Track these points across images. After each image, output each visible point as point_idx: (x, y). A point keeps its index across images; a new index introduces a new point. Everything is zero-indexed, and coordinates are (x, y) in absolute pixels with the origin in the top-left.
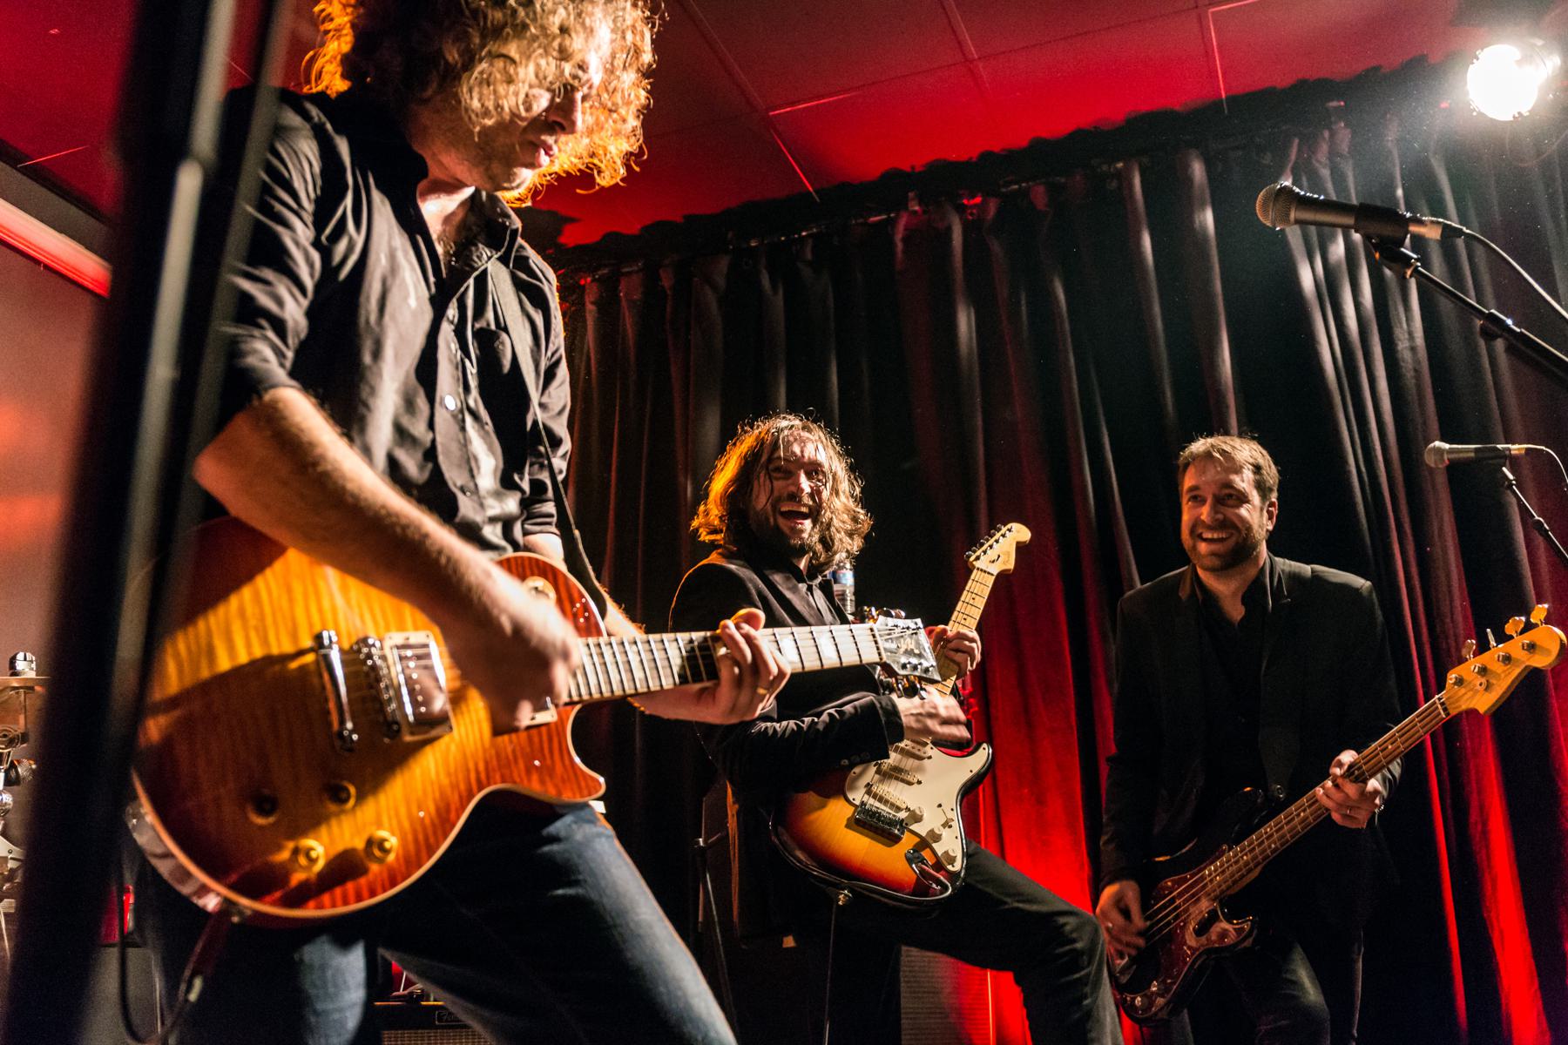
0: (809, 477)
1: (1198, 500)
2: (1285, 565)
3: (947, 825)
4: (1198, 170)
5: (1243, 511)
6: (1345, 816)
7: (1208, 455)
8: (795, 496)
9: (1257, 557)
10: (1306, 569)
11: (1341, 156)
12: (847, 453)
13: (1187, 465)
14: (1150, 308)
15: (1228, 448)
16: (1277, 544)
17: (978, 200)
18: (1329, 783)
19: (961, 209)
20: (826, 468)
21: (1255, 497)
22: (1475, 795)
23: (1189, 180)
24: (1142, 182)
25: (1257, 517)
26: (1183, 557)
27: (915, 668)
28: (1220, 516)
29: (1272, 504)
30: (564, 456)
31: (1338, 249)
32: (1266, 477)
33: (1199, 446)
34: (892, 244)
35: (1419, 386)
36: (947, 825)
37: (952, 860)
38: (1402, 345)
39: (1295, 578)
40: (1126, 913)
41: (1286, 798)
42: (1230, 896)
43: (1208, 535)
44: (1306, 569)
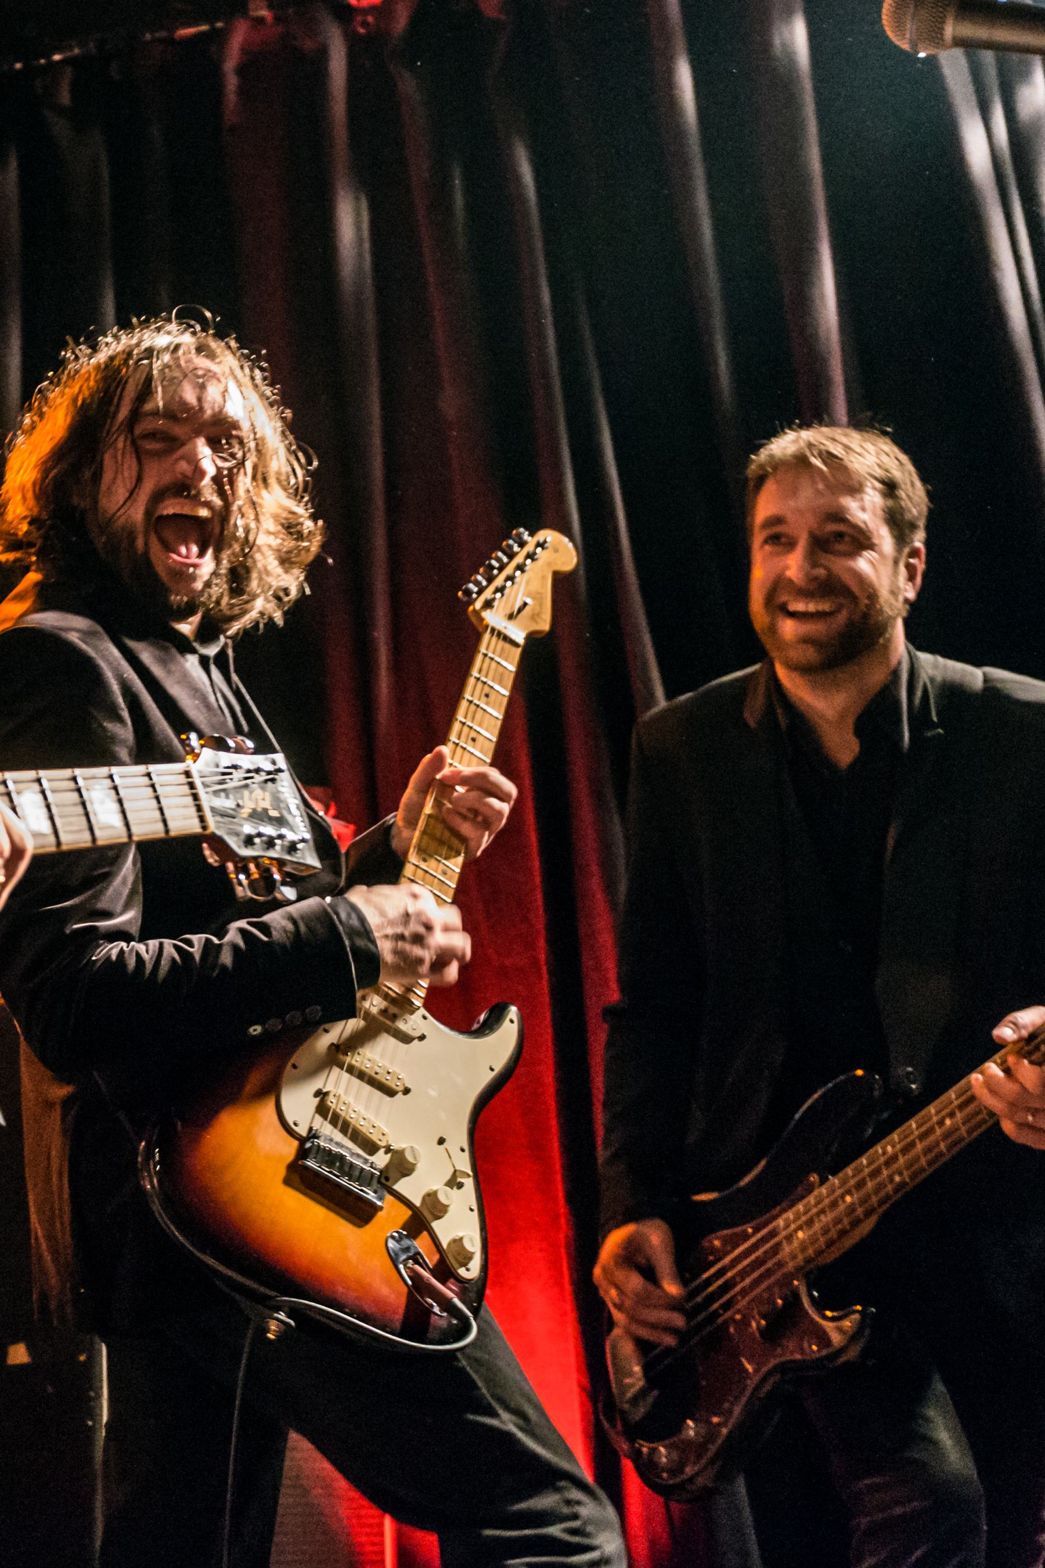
0: (214, 444)
1: (780, 540)
2: (935, 666)
3: (454, 1183)
5: (863, 564)
6: (1022, 1125)
7: (801, 461)
8: (185, 487)
9: (886, 647)
10: (974, 676)
12: (285, 400)
14: (689, 194)
15: (837, 450)
18: (993, 1068)
20: (245, 425)
25: (887, 574)
26: (751, 647)
27: (270, 843)
28: (821, 572)
29: (914, 553)
32: (905, 503)
33: (785, 444)
36: (454, 1183)
37: (465, 1259)
39: (953, 693)
43: (799, 606)
44: (974, 676)
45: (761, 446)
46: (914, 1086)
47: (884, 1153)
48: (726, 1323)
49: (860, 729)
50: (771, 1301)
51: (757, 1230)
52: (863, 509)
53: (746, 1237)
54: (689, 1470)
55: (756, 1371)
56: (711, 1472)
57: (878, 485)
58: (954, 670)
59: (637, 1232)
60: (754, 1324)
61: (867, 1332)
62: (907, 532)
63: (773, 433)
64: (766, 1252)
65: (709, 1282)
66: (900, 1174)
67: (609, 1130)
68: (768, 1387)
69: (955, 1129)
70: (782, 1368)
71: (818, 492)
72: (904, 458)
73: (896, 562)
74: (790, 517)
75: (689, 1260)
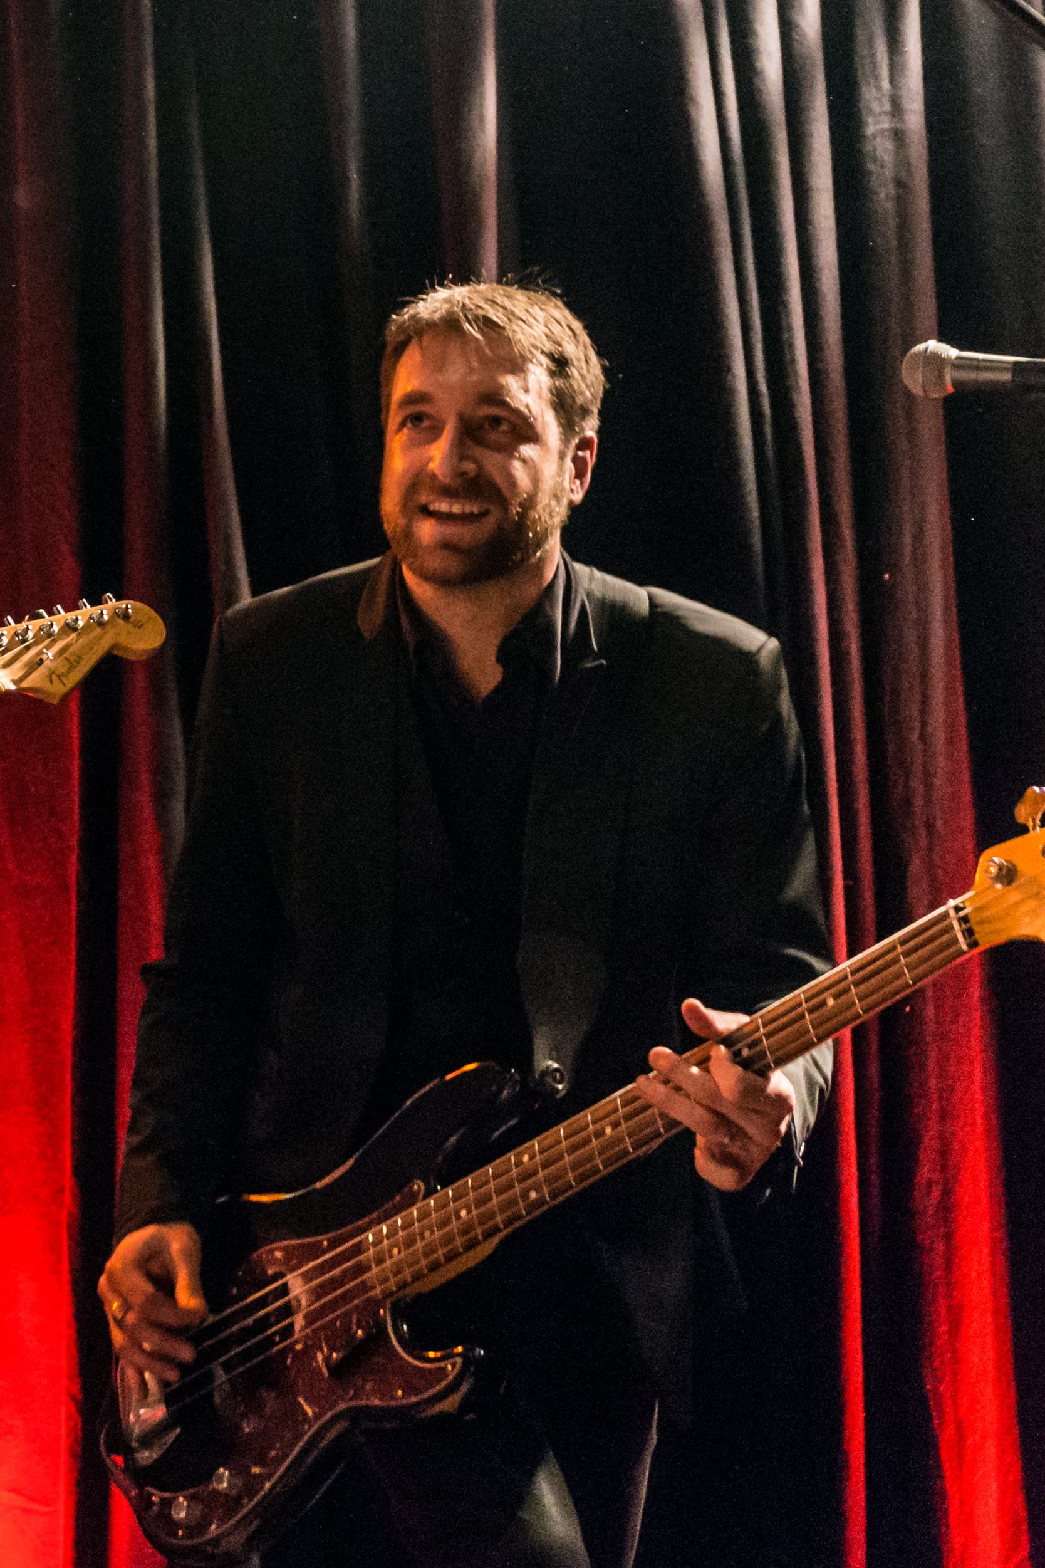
1: (421, 418)
2: (596, 582)
7: (450, 325)
10: (638, 596)
13: (401, 348)
16: (586, 535)
22: (933, 1123)
25: (551, 475)
26: (368, 536)
28: (469, 467)
29: (585, 444)
32: (577, 382)
33: (433, 304)
34: (291, 1199)
35: (904, 227)
38: (876, 125)
39: (614, 614)
40: (165, 1284)
41: (570, 1092)
42: (420, 1297)
43: (444, 506)
44: (638, 596)
45: (405, 304)
46: (560, 1087)
47: (519, 1163)
48: (283, 1353)
49: (504, 655)
50: (347, 1330)
51: (333, 1245)
52: (527, 391)
55: (317, 1417)
56: (240, 1537)
57: (545, 361)
58: (614, 588)
59: (153, 1238)
60: (320, 1357)
61: (464, 1388)
62: (577, 419)
63: (418, 289)
64: (344, 1272)
65: (263, 1302)
66: (538, 1189)
67: (137, 1112)
68: (331, 1435)
69: (617, 1141)
70: (354, 1415)
71: (471, 370)
72: (577, 325)
73: (562, 456)
74: (439, 395)
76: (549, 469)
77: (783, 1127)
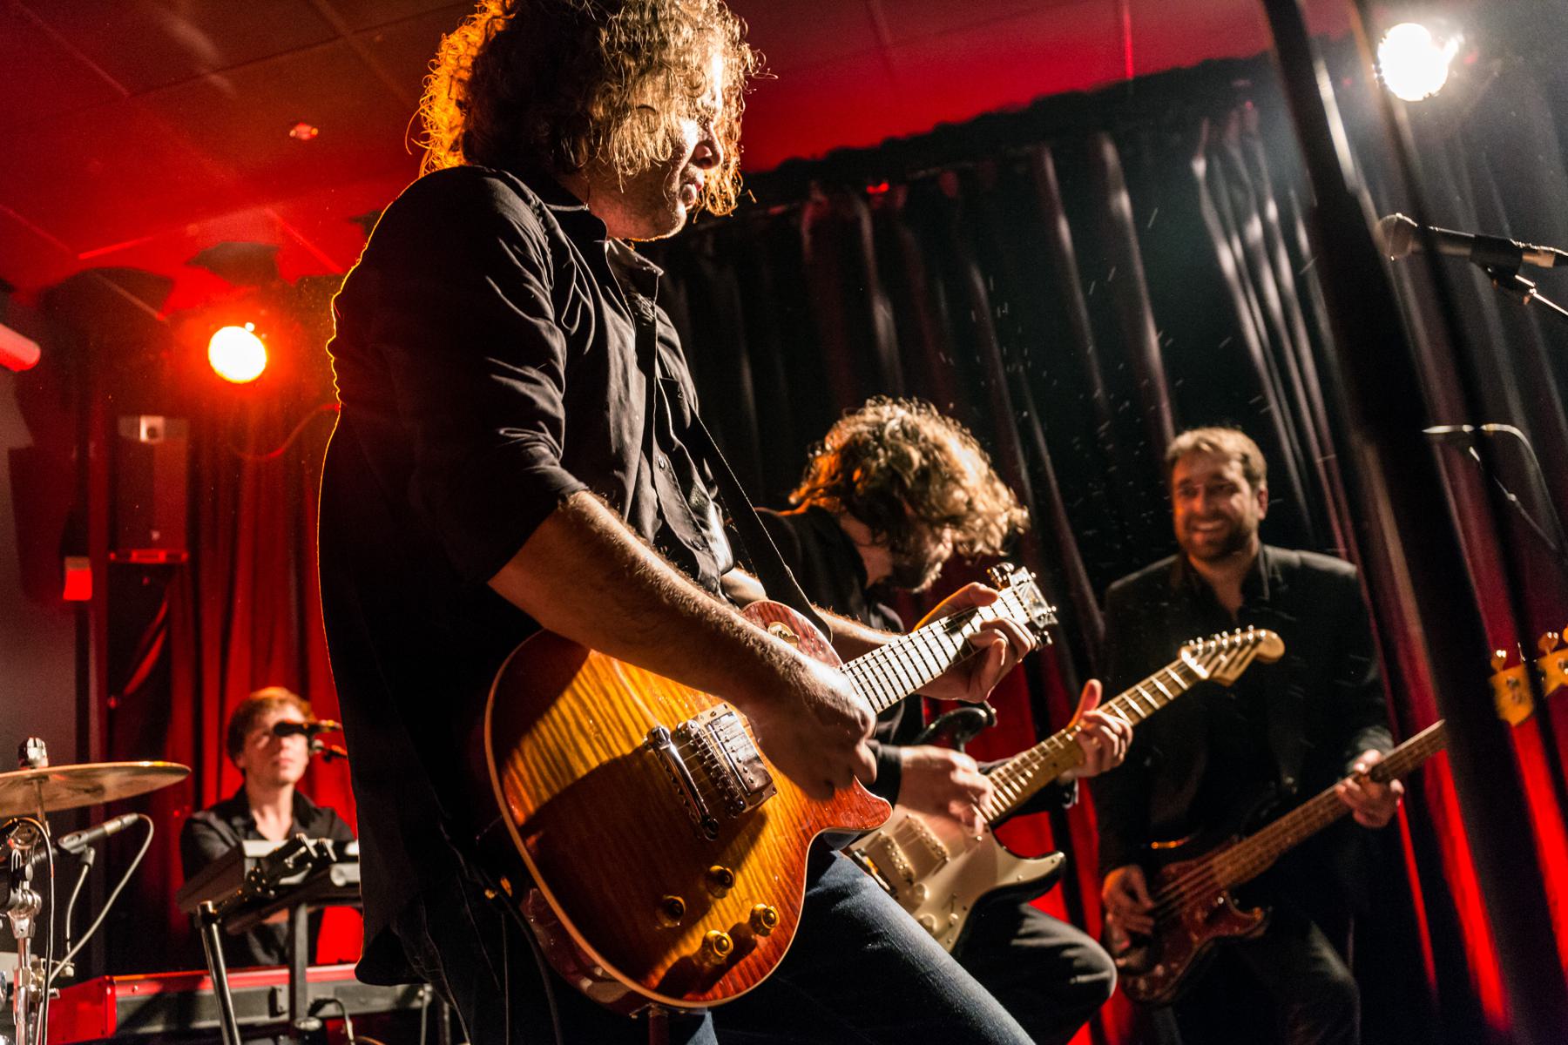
1: (1190, 493)
2: (1275, 553)
4: (1110, 153)
5: (1235, 501)
6: (1369, 817)
7: (1196, 449)
9: (1250, 545)
10: (1294, 556)
11: (1250, 135)
16: (1273, 531)
17: (884, 187)
19: (867, 198)
21: (1245, 486)
23: (1103, 164)
24: (1057, 167)
25: (1248, 505)
29: (1261, 493)
30: (932, 565)
31: (1255, 230)
39: (1286, 567)
40: (1132, 894)
51: (1199, 864)
53: (1192, 868)
54: (1157, 992)
65: (1168, 893)
69: (1324, 816)
70: (1217, 939)
75: (1154, 881)
76: (1247, 503)
77: (542, 424)
